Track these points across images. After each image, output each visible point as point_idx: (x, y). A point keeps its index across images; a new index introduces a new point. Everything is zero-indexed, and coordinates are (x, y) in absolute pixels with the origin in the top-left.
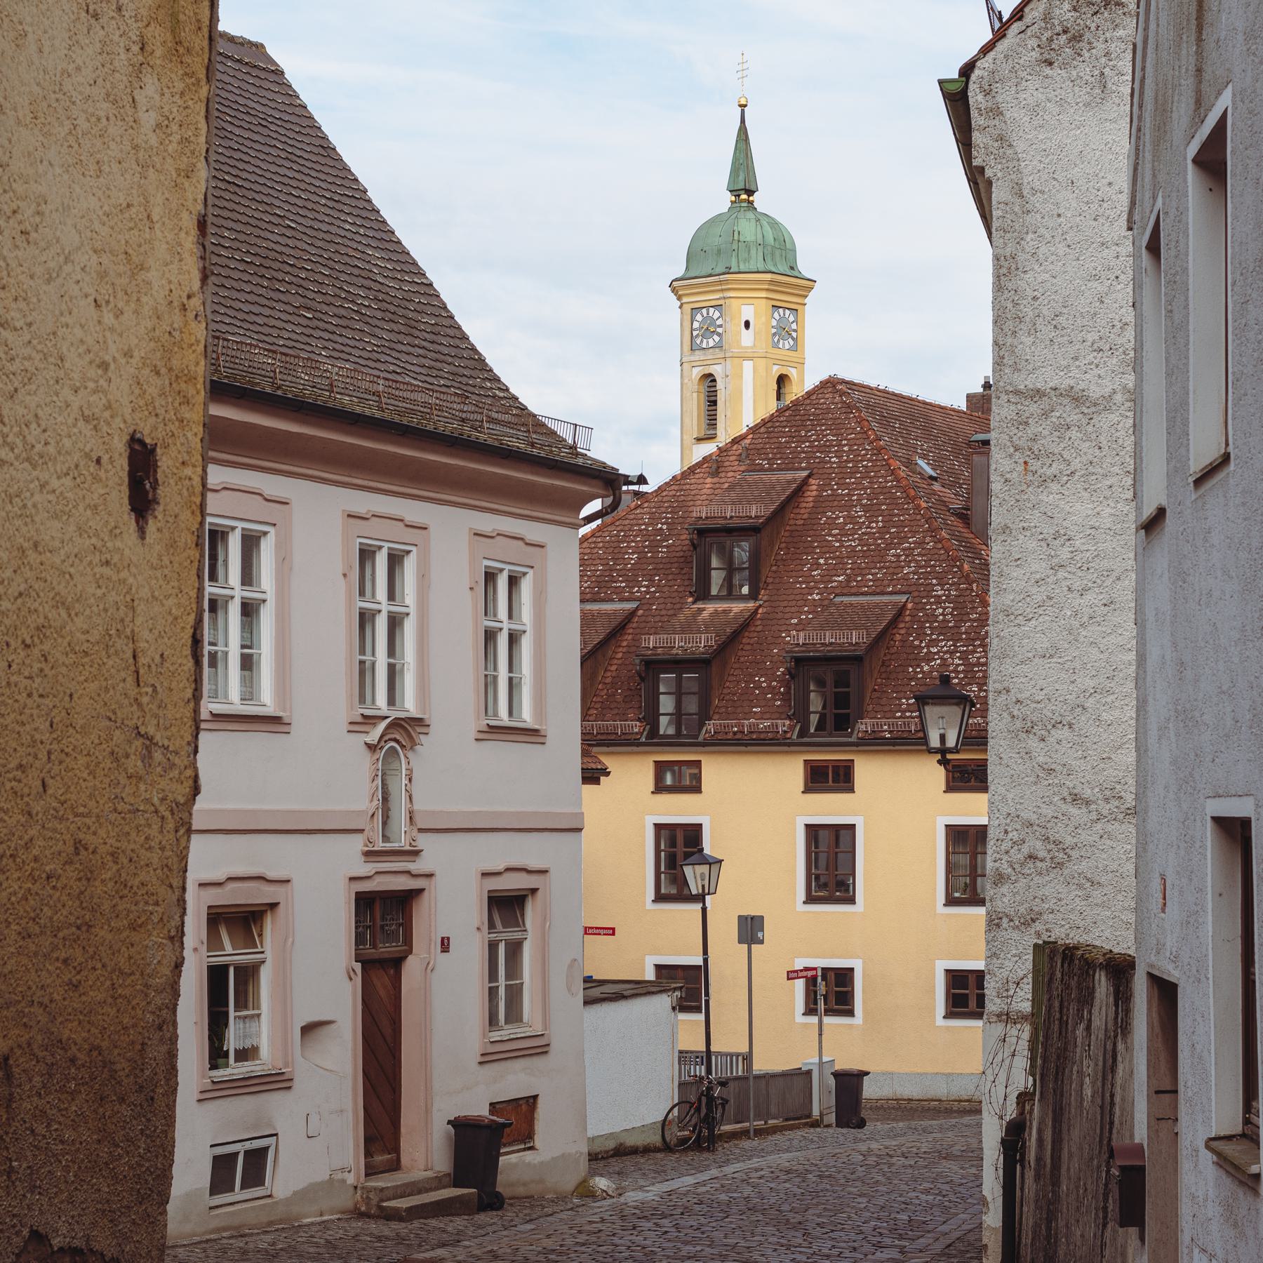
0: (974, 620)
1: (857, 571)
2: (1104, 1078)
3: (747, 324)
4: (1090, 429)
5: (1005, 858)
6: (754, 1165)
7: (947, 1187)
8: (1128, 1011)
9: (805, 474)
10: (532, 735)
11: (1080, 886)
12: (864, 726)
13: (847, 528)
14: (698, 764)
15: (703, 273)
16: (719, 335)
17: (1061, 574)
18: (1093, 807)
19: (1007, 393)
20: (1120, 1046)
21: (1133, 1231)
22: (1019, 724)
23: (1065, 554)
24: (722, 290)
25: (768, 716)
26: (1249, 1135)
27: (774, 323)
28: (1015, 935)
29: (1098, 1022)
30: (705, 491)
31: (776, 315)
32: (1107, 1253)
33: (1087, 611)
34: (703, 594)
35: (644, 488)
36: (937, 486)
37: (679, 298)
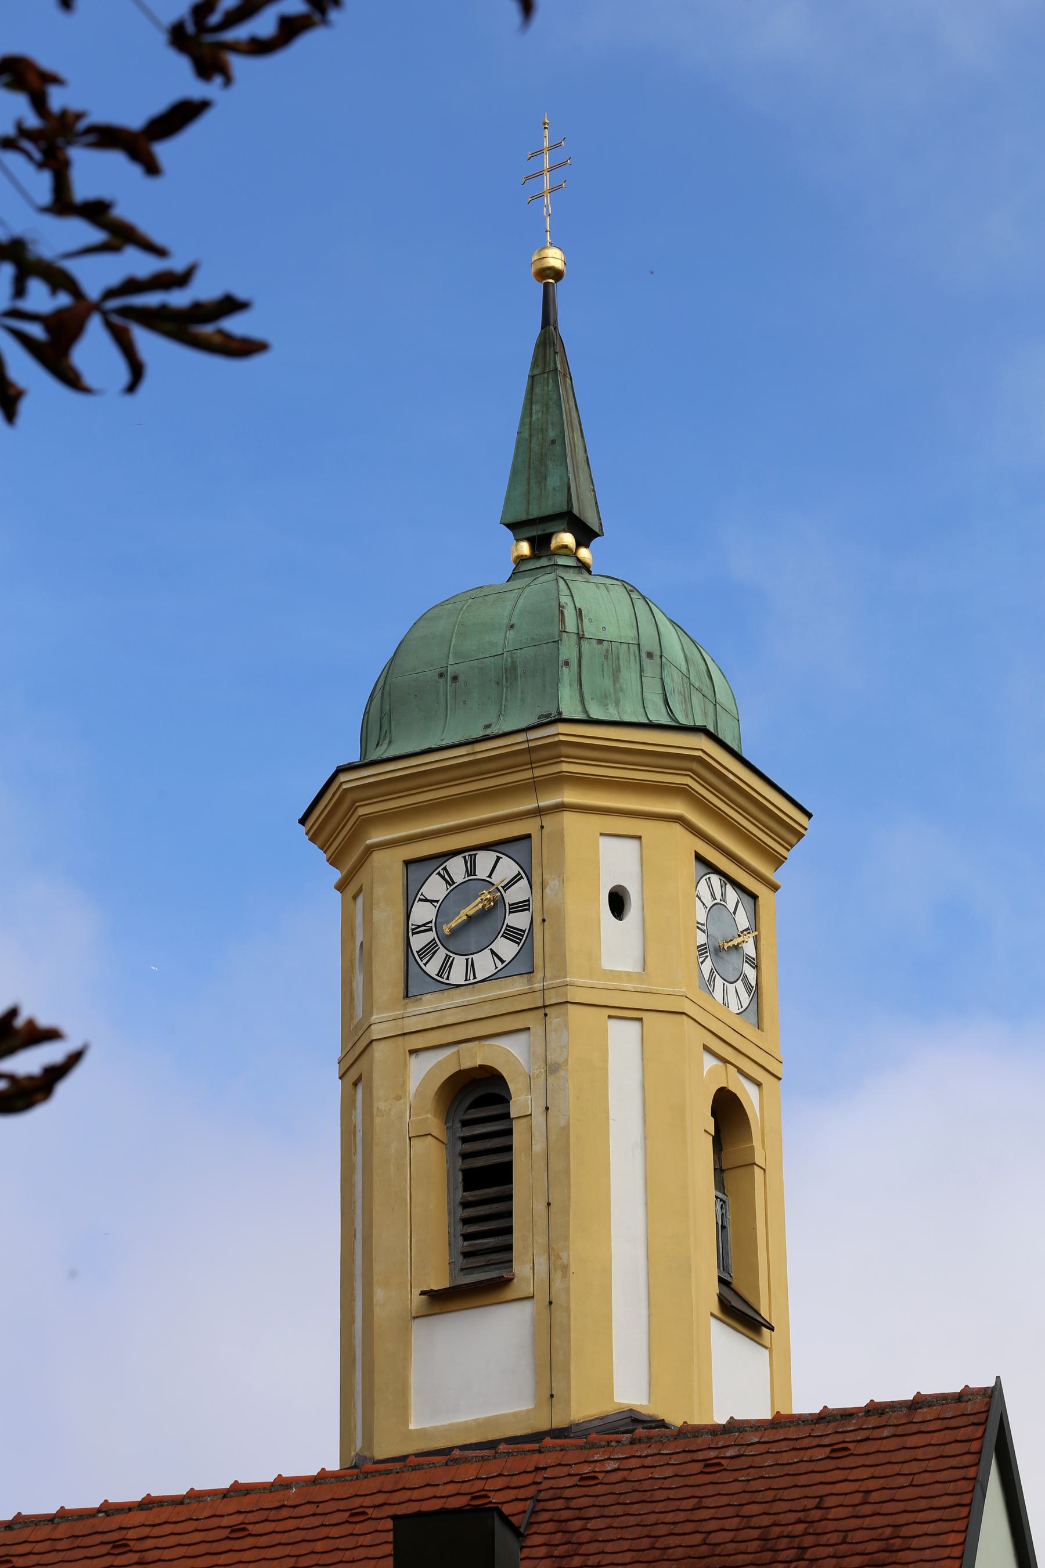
16: (513, 934)
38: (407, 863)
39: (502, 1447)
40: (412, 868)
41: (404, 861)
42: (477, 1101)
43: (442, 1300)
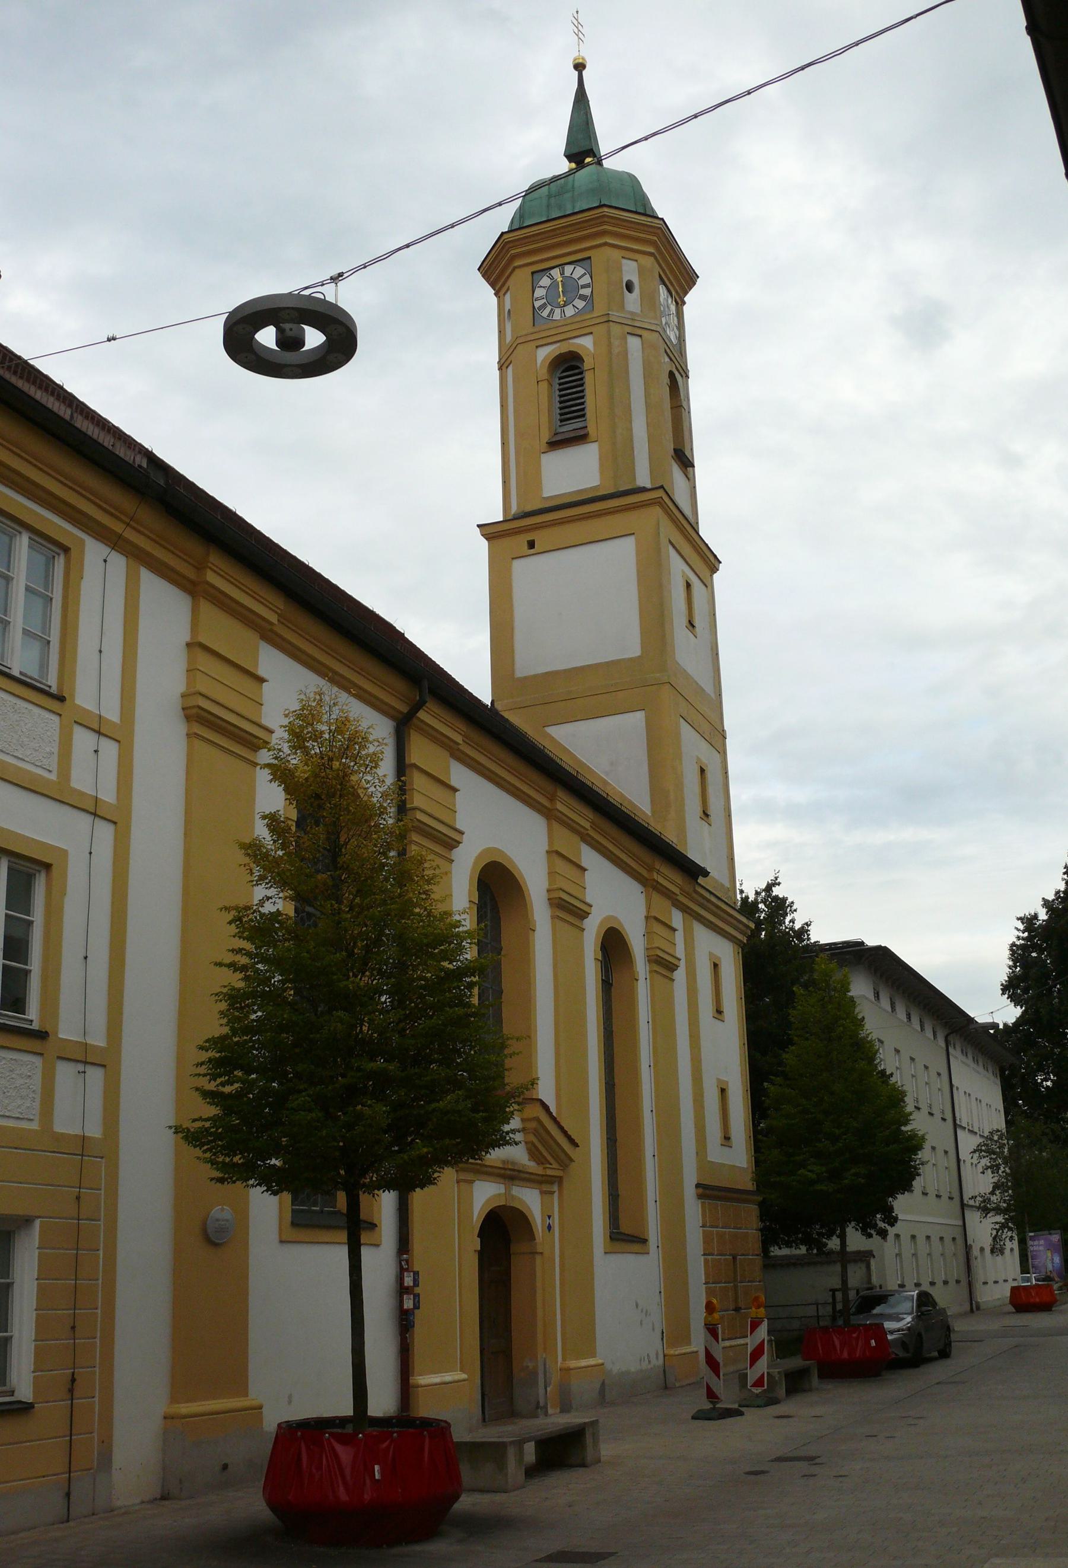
16: (583, 297)
38: (533, 273)
40: (535, 276)
41: (51, 865)
42: (568, 367)
43: (556, 444)
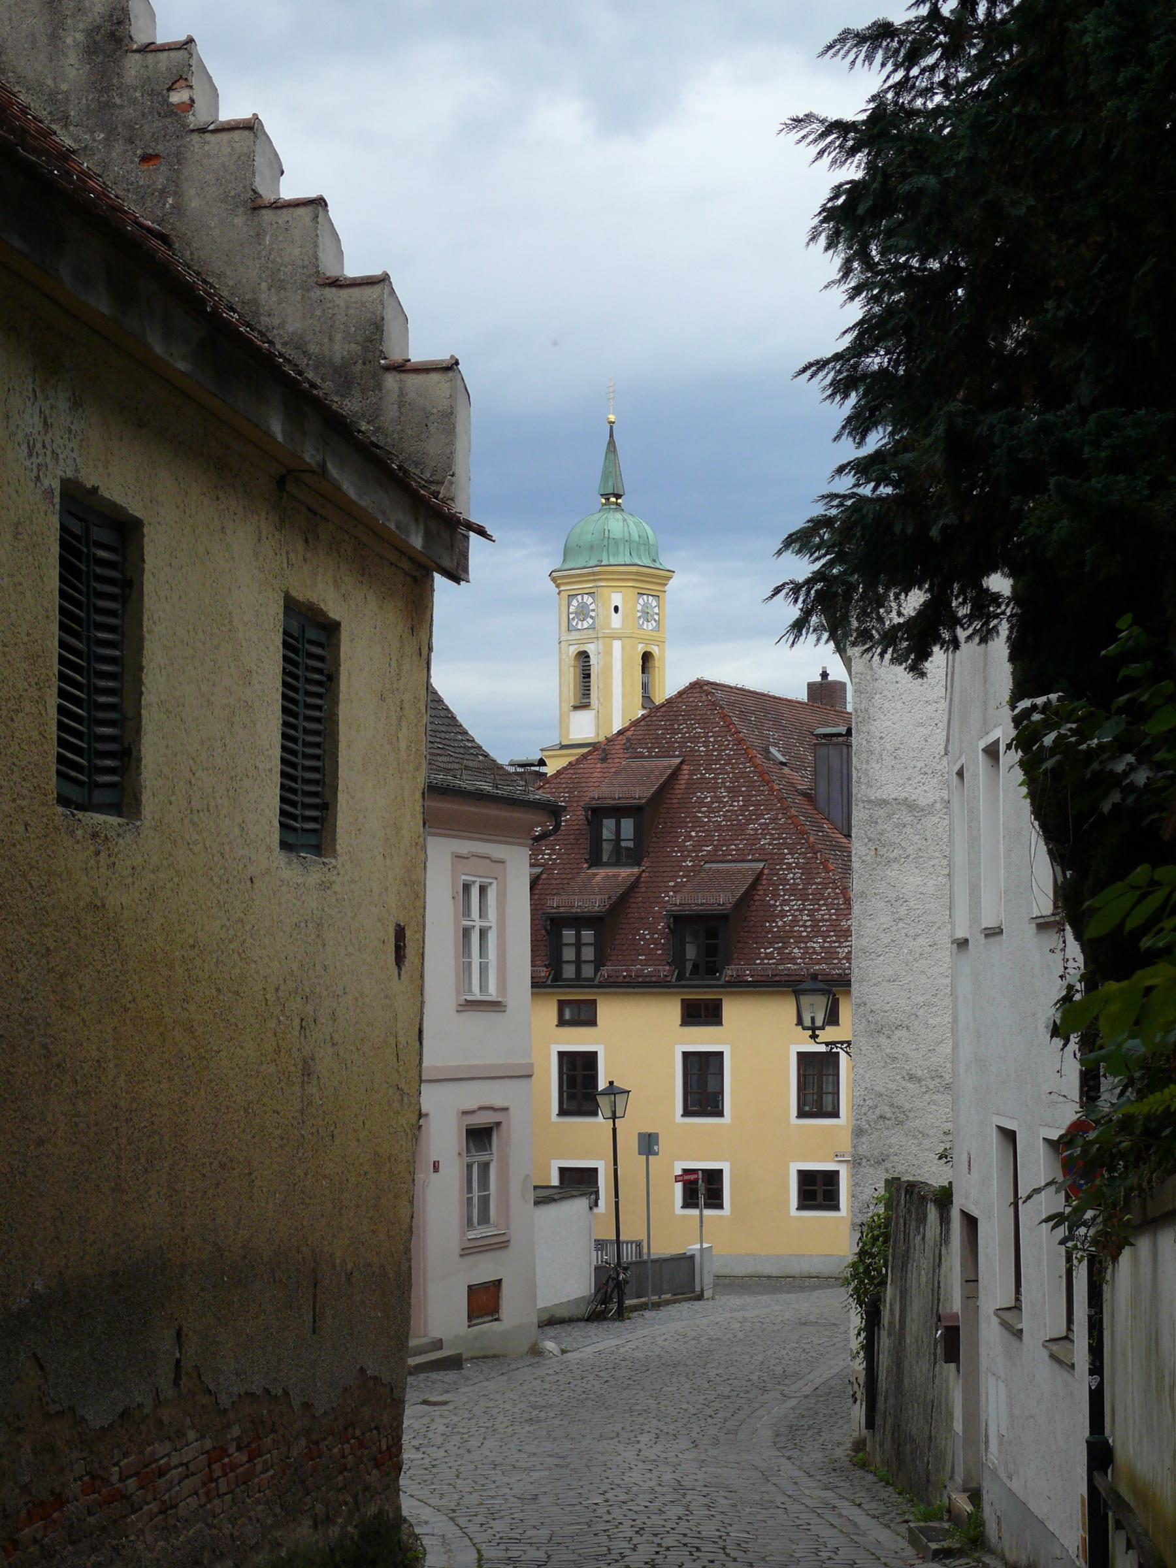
0: (819, 884)
1: (723, 842)
2: (934, 1271)
3: (616, 609)
4: (919, 827)
5: (864, 1118)
6: (660, 1331)
7: (809, 1346)
8: (948, 1230)
9: (678, 760)
10: (496, 1006)
11: (915, 1137)
12: (730, 971)
13: (713, 807)
14: (594, 1003)
15: (578, 566)
16: (592, 617)
17: (901, 925)
18: (923, 1083)
19: (863, 802)
20: (943, 1252)
21: (953, 1366)
22: (873, 1027)
23: (903, 911)
24: (595, 580)
25: (651, 962)
26: (1017, 1307)
27: (639, 607)
28: (871, 1170)
29: (930, 1235)
30: (595, 774)
31: (641, 601)
32: (937, 1382)
33: (919, 950)
34: (595, 860)
35: (543, 769)
36: (786, 770)
37: (558, 586)
39: (422, 855)
